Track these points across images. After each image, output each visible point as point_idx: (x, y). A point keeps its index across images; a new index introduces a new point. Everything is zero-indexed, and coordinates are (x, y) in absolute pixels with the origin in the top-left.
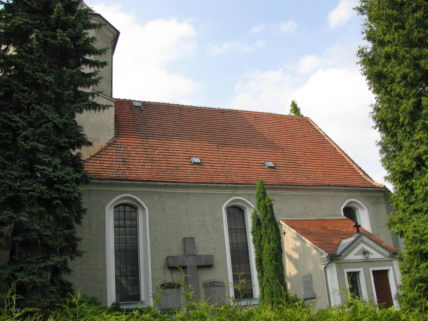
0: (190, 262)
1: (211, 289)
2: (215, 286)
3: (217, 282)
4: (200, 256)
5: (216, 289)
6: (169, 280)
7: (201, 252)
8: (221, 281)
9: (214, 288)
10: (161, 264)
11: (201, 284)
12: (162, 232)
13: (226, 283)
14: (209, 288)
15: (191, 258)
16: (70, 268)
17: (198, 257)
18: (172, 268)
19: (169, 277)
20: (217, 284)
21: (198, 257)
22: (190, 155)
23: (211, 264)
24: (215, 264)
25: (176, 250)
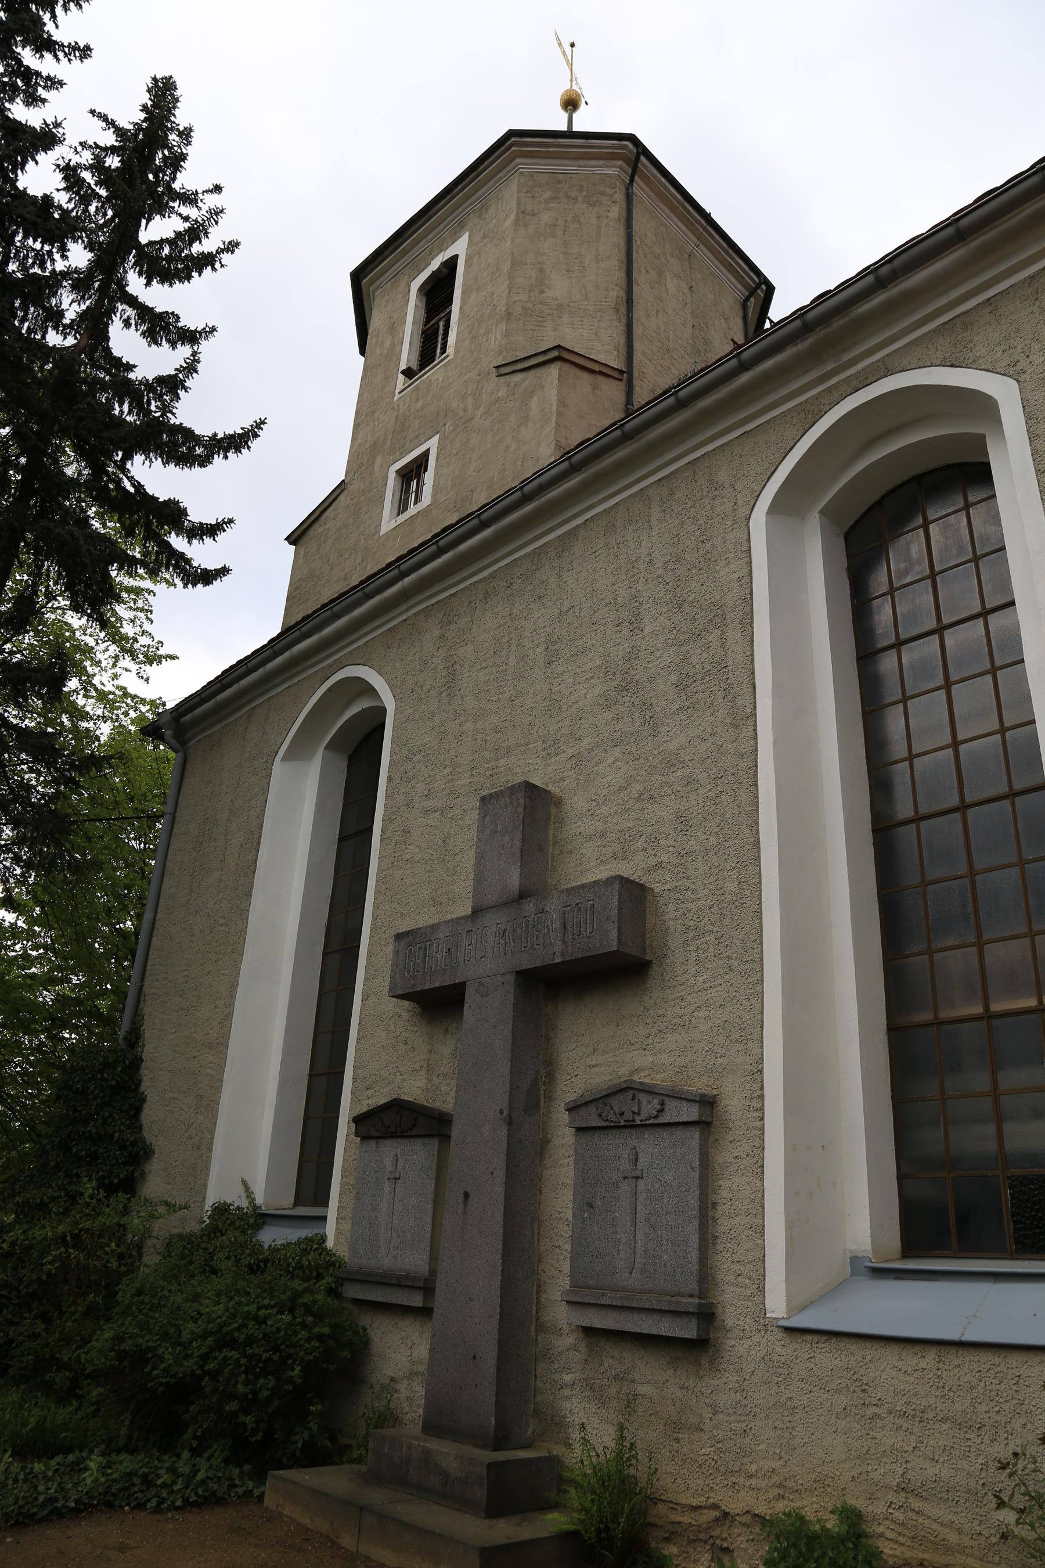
2: (631, 1126)
9: (633, 1140)
20: (649, 1107)
22: (744, 797)
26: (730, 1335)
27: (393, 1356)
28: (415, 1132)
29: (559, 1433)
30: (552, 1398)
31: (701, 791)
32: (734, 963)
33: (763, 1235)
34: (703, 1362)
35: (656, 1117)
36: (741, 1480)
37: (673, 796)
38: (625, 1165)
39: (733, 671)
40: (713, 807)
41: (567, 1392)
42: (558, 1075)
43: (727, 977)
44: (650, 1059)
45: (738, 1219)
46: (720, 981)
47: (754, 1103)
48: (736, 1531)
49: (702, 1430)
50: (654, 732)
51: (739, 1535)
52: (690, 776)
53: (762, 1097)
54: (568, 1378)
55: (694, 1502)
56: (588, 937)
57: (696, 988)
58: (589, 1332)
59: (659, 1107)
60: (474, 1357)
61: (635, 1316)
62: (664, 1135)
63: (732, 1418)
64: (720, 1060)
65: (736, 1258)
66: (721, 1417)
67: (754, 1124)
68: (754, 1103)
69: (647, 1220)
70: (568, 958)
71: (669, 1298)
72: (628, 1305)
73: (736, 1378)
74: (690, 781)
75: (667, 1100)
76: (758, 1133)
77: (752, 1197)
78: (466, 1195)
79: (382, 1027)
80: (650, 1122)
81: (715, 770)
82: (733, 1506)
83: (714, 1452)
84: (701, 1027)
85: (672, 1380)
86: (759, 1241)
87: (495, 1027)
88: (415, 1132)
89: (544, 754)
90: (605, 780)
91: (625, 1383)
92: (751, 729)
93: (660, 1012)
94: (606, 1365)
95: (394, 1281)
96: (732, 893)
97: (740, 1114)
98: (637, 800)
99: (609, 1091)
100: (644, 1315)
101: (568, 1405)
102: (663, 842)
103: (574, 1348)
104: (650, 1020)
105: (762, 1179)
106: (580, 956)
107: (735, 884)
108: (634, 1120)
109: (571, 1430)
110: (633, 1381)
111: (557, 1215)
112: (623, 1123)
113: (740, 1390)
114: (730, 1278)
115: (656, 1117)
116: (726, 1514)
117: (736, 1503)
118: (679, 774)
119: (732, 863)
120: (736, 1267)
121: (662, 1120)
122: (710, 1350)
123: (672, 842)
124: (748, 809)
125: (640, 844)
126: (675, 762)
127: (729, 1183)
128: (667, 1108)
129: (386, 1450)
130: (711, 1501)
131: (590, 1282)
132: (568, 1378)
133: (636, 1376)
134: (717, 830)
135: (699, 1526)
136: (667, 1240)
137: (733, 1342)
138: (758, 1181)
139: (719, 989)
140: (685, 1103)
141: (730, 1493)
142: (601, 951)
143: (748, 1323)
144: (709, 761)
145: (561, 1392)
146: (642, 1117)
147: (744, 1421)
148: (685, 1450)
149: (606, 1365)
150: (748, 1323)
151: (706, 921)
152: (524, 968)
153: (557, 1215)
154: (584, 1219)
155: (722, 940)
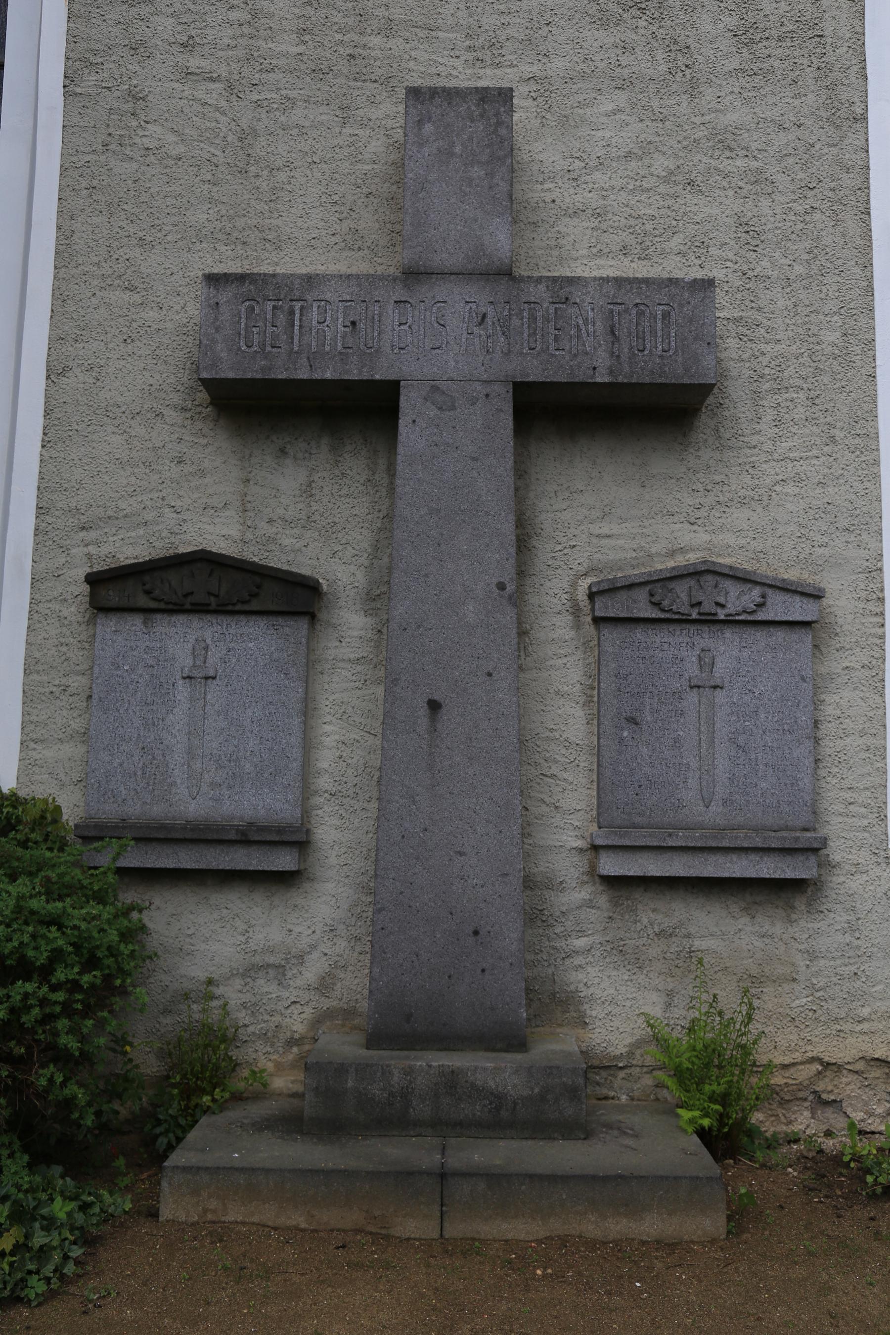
0: (444, 355)
1: (678, 649)
2: (709, 621)
3: (744, 579)
4: (563, 288)
5: (728, 650)
6: (220, 535)
7: (586, 252)
8: (791, 575)
9: (705, 639)
10: (150, 369)
11: (557, 589)
12: (195, 63)
13: (841, 602)
14: (639, 633)
15: (458, 302)
16: (202, 975)
17: (540, 292)
18: (257, 407)
19: (222, 501)
20: (738, 600)
21: (540, 292)
22: (852, 226)
23: (676, 372)
24: (737, 391)
25: (315, 233)
26: (837, 871)
27: (203, 947)
28: (254, 606)
29: (564, 1012)
30: (550, 971)
31: (778, 197)
32: (839, 434)
33: (885, 758)
34: (797, 904)
35: (753, 612)
36: (847, 1027)
37: (731, 193)
38: (692, 670)
39: (835, 48)
40: (800, 226)
41: (578, 960)
42: (534, 542)
43: (826, 449)
44: (706, 537)
45: (848, 740)
46: (815, 452)
47: (872, 607)
48: (844, 1080)
49: (794, 980)
50: (693, 90)
51: (848, 1084)
52: (759, 171)
53: (882, 600)
54: (580, 943)
55: (787, 1060)
56: (661, 357)
57: (776, 456)
58: (614, 883)
59: (759, 600)
60: (476, 933)
61: (720, 858)
62: (760, 636)
63: (839, 962)
64: (820, 551)
65: (846, 784)
66: (822, 962)
67: (873, 631)
68: (872, 607)
69: (733, 741)
70: (620, 379)
71: (773, 834)
72: (714, 845)
73: (846, 917)
74: (758, 178)
75: (770, 592)
76: (878, 642)
77: (871, 714)
78: (434, 706)
79: (110, 429)
80: (740, 618)
81: (801, 175)
82: (841, 1055)
83: (812, 1002)
84: (788, 505)
85: (749, 929)
86: (879, 765)
87: (474, 459)
88: (254, 606)
89: (470, 56)
90: (600, 134)
91: (674, 939)
92: (862, 138)
93: (718, 478)
94: (645, 921)
95: (232, 836)
96: (834, 345)
97: (850, 618)
98: (666, 180)
99: (675, 573)
100: (735, 857)
101: (581, 976)
102: (714, 251)
103: (589, 904)
104: (700, 487)
105: (882, 695)
106: (647, 380)
107: (838, 334)
108: (715, 614)
109: (586, 1006)
110: (688, 936)
111: (548, 734)
112: (694, 616)
113: (851, 928)
114: (839, 807)
115: (753, 612)
116: (827, 1065)
117: (843, 1052)
118: (739, 163)
119: (831, 306)
120: (848, 795)
121: (761, 616)
122: (809, 890)
123: (731, 256)
124: (859, 242)
125: (675, 243)
126: (733, 144)
127: (836, 698)
128: (769, 601)
129: (350, 1084)
130: (810, 1054)
131: (637, 820)
132: (580, 943)
133: (692, 930)
134: (806, 257)
135: (801, 1083)
136: (766, 765)
137: (841, 879)
138: (877, 697)
139: (815, 461)
140: (798, 598)
141: (835, 1043)
142: (686, 381)
143: (864, 857)
144: (791, 160)
145: (568, 962)
146: (726, 611)
147: (855, 963)
148: (770, 1006)
149: (645, 921)
150: (864, 857)
151: (790, 371)
152: (531, 379)
153: (548, 734)
154: (621, 740)
155: (817, 401)
